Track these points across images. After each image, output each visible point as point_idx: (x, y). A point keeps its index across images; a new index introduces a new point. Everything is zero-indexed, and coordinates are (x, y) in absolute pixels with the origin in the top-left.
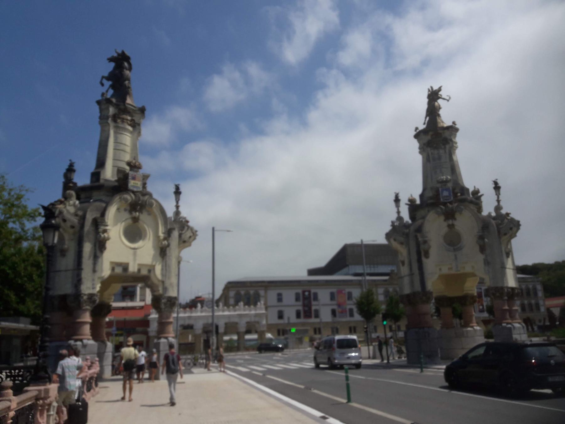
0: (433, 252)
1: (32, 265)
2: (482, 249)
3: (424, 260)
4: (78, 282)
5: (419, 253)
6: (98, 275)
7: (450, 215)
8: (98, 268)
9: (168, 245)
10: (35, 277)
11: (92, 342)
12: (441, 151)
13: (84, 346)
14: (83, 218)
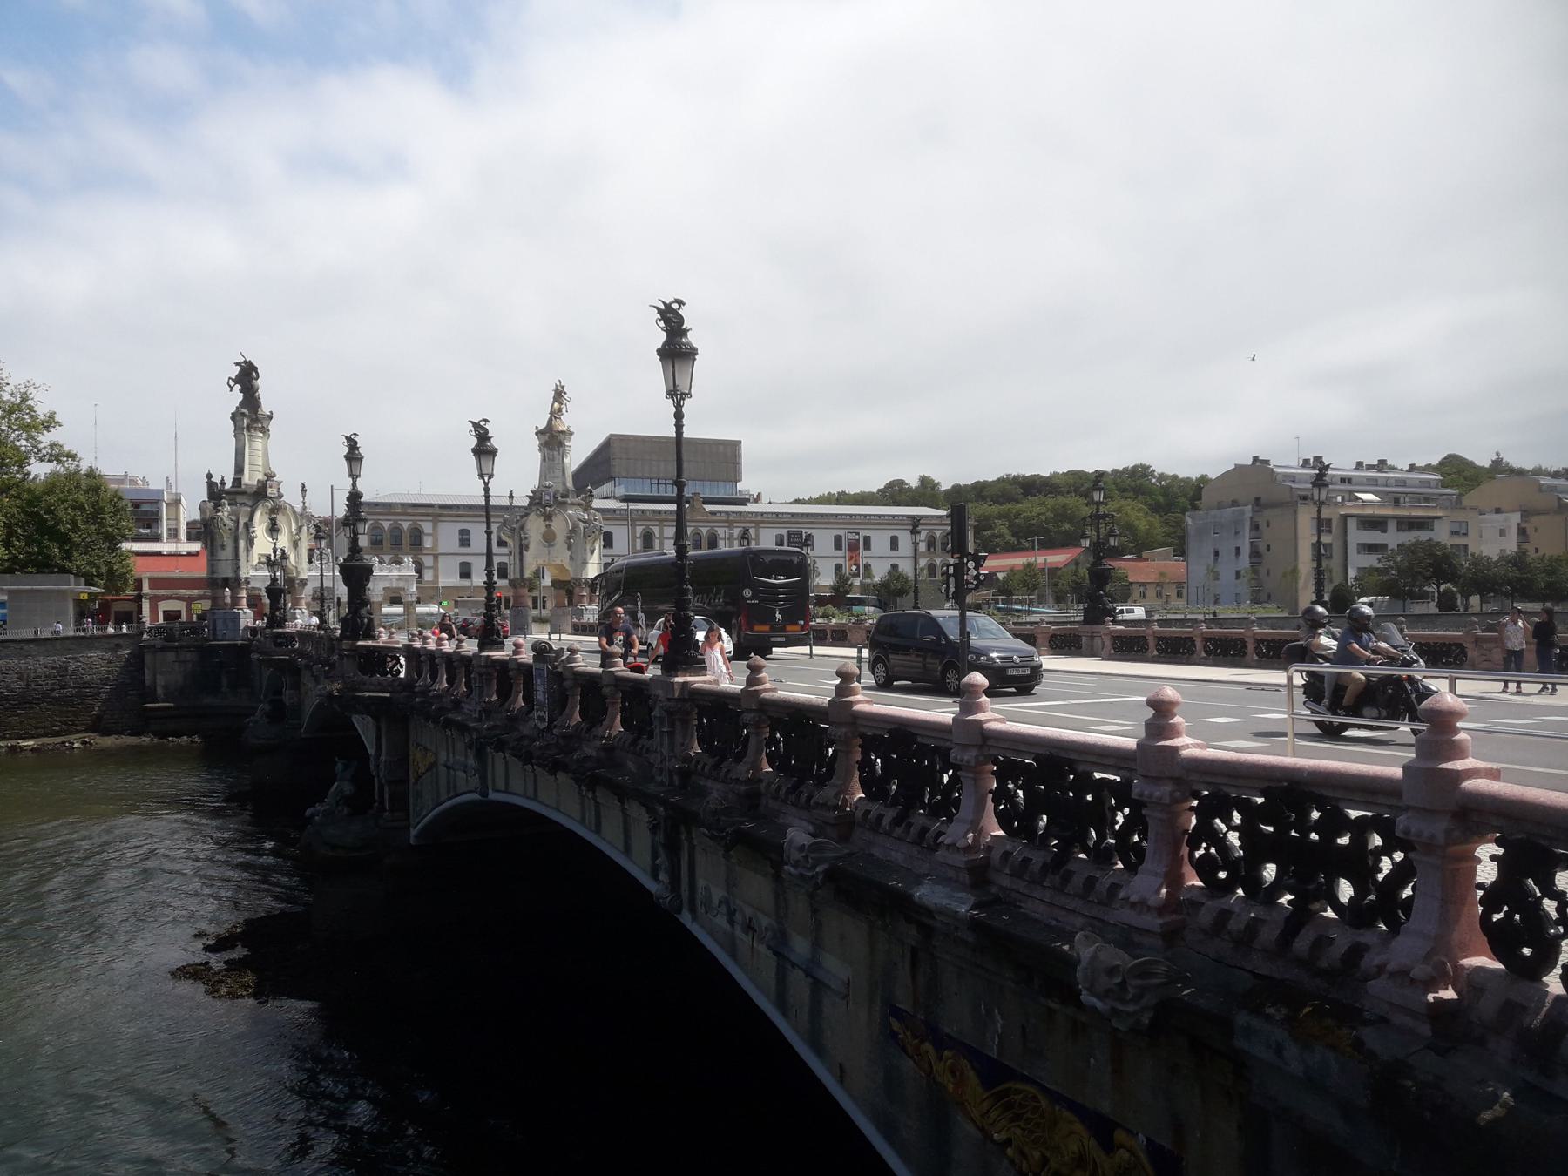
0: (532, 547)
1: (74, 508)
2: (569, 547)
3: (524, 552)
4: (237, 569)
5: (521, 546)
6: (250, 563)
7: (548, 517)
8: (250, 559)
9: (300, 539)
10: (80, 524)
11: (248, 610)
12: (555, 453)
13: (245, 613)
14: (237, 522)
